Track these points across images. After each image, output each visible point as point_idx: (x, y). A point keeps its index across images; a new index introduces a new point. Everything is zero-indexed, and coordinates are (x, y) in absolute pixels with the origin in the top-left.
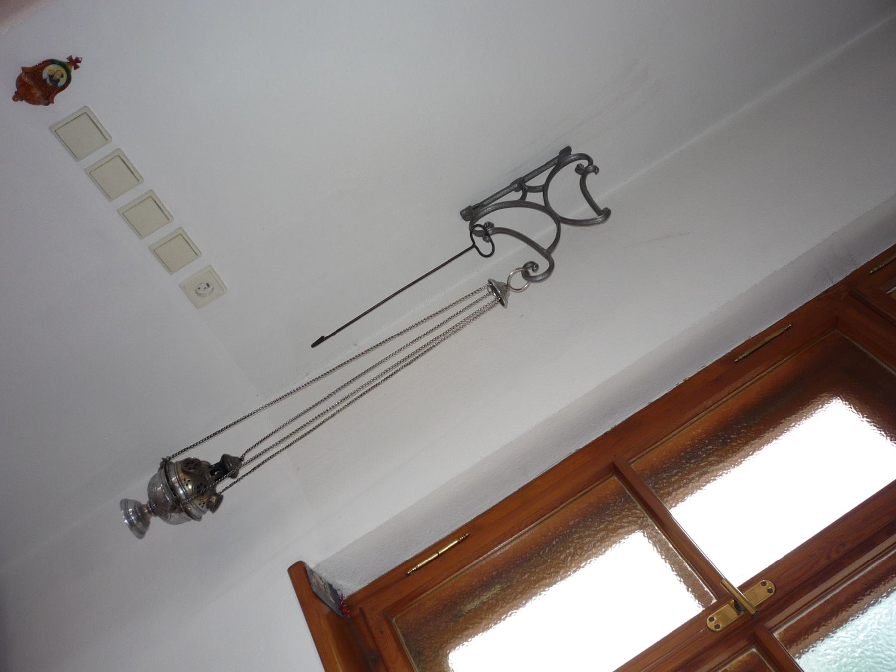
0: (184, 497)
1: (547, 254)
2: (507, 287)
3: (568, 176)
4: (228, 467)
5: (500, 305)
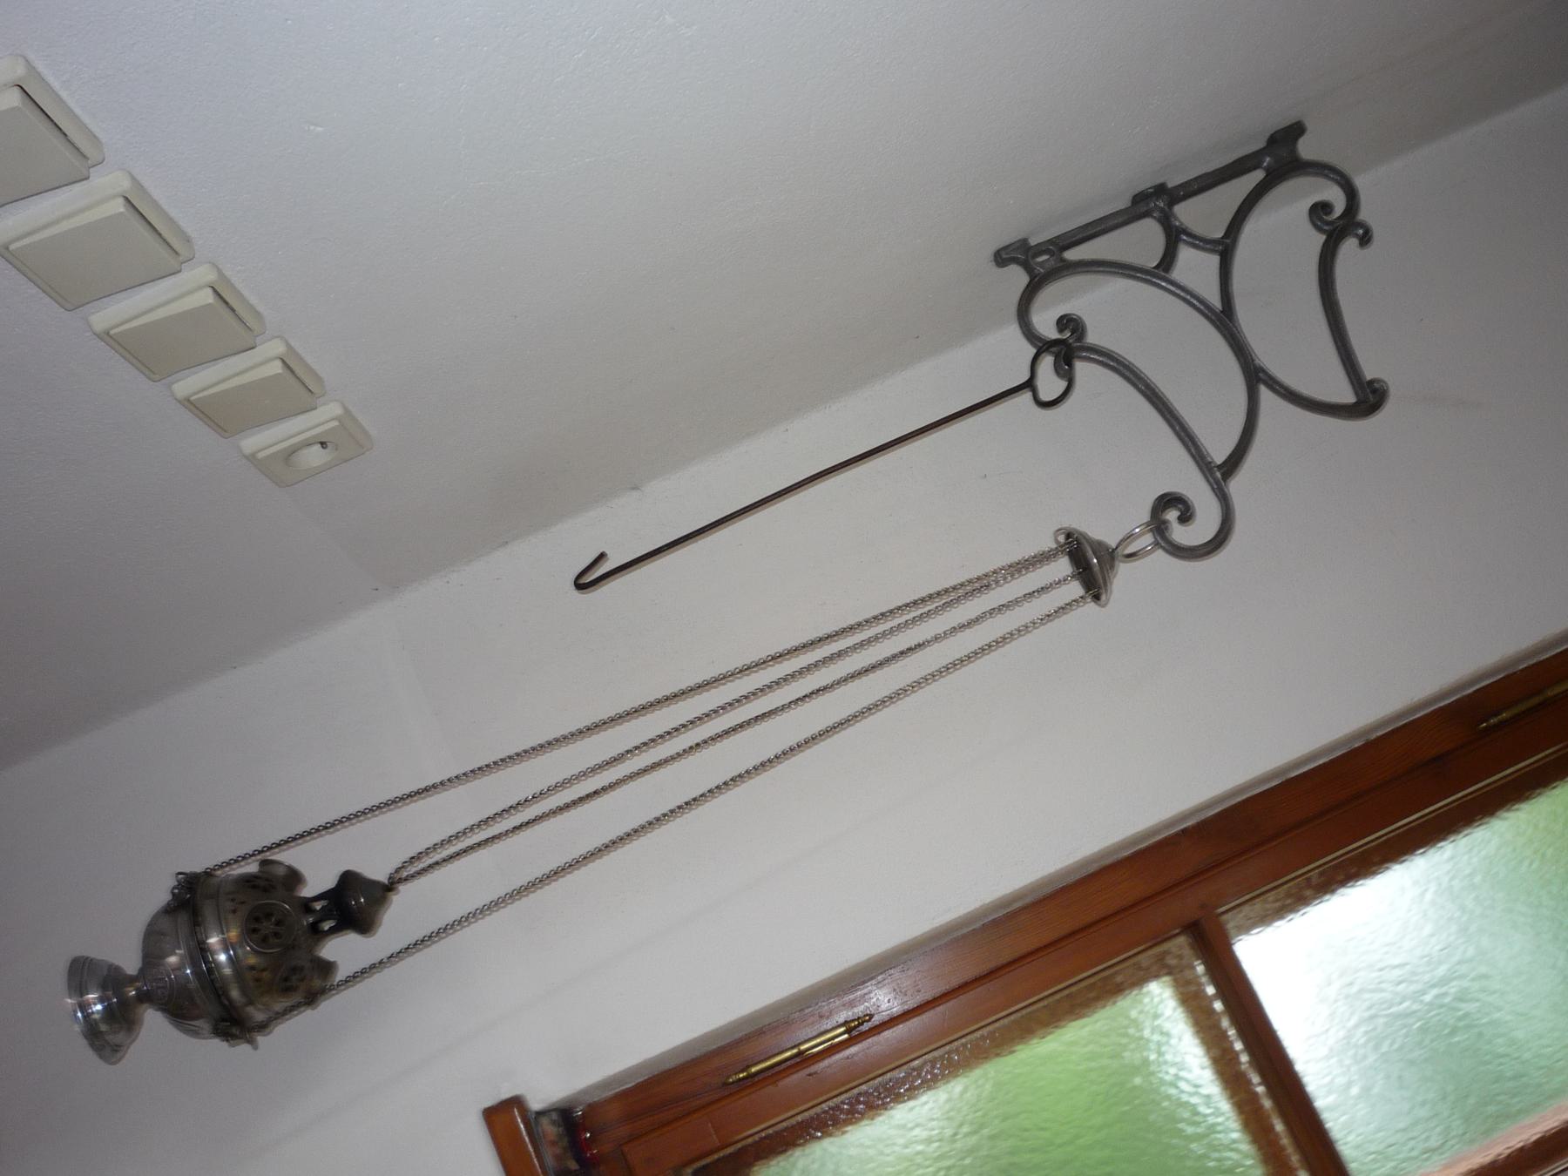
0: (227, 971)
1: (1221, 474)
2: (1109, 556)
3: (1282, 229)
4: (354, 903)
5: (1307, 149)
